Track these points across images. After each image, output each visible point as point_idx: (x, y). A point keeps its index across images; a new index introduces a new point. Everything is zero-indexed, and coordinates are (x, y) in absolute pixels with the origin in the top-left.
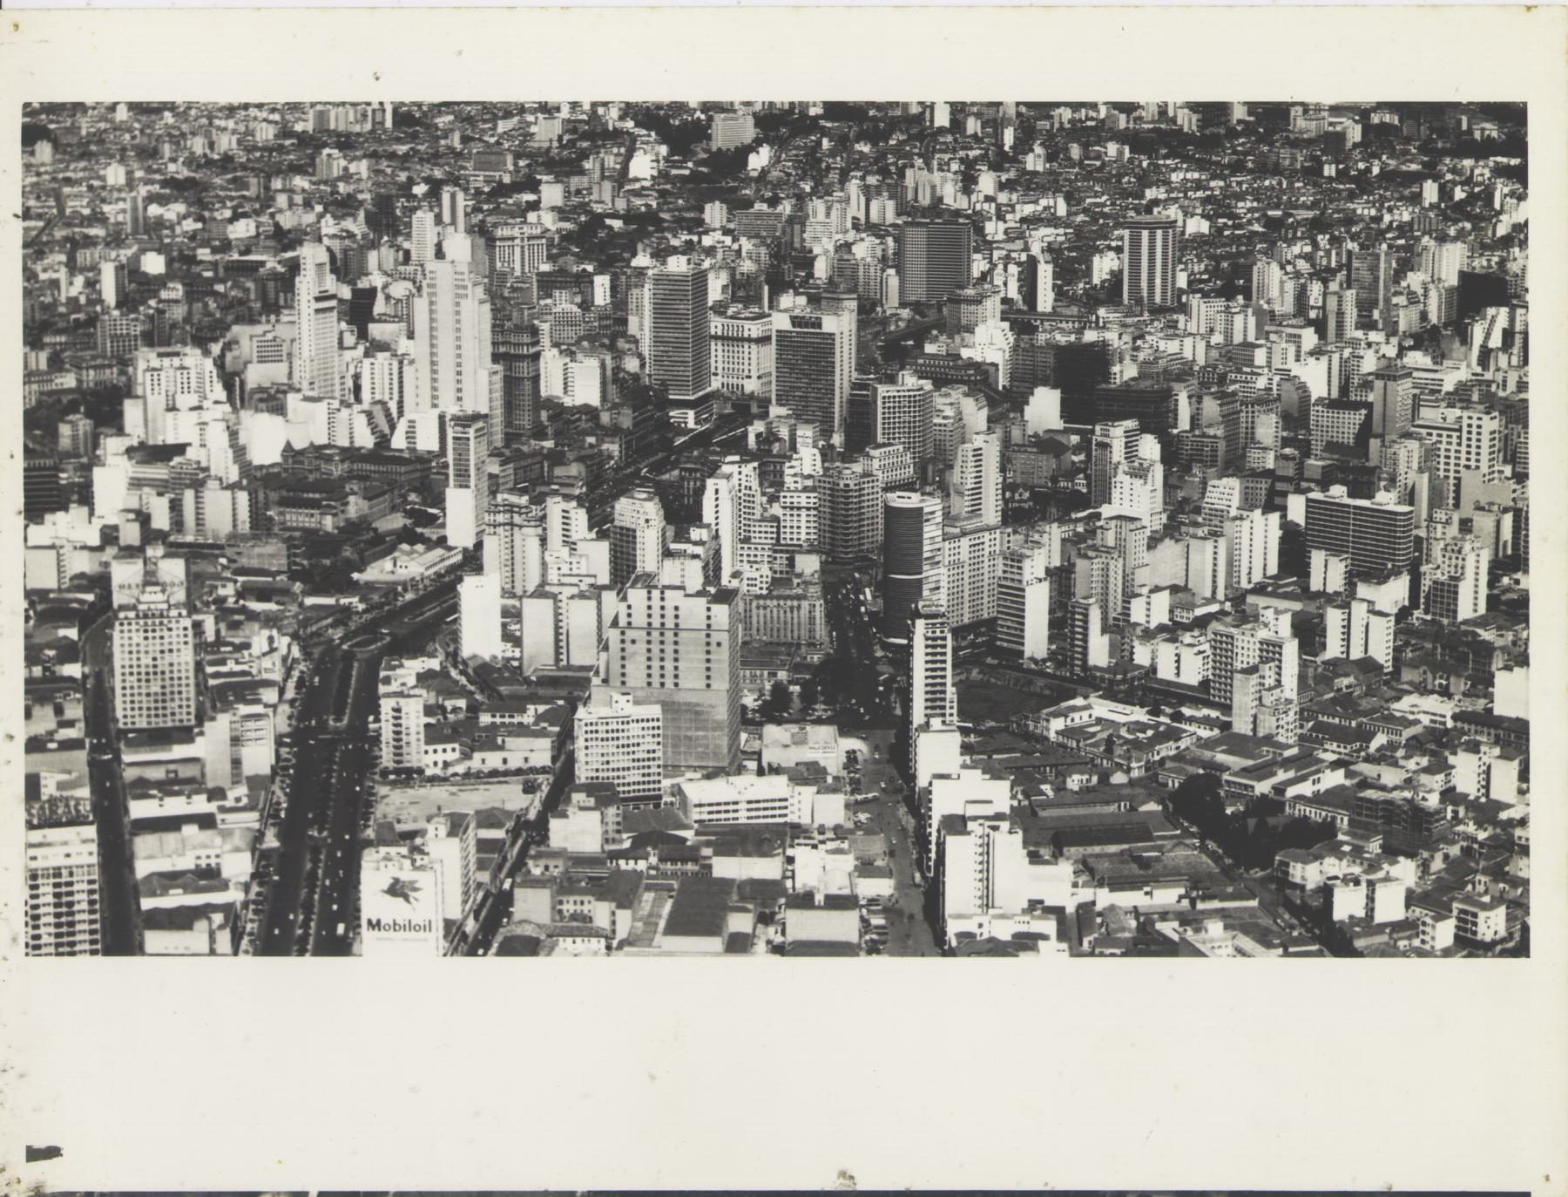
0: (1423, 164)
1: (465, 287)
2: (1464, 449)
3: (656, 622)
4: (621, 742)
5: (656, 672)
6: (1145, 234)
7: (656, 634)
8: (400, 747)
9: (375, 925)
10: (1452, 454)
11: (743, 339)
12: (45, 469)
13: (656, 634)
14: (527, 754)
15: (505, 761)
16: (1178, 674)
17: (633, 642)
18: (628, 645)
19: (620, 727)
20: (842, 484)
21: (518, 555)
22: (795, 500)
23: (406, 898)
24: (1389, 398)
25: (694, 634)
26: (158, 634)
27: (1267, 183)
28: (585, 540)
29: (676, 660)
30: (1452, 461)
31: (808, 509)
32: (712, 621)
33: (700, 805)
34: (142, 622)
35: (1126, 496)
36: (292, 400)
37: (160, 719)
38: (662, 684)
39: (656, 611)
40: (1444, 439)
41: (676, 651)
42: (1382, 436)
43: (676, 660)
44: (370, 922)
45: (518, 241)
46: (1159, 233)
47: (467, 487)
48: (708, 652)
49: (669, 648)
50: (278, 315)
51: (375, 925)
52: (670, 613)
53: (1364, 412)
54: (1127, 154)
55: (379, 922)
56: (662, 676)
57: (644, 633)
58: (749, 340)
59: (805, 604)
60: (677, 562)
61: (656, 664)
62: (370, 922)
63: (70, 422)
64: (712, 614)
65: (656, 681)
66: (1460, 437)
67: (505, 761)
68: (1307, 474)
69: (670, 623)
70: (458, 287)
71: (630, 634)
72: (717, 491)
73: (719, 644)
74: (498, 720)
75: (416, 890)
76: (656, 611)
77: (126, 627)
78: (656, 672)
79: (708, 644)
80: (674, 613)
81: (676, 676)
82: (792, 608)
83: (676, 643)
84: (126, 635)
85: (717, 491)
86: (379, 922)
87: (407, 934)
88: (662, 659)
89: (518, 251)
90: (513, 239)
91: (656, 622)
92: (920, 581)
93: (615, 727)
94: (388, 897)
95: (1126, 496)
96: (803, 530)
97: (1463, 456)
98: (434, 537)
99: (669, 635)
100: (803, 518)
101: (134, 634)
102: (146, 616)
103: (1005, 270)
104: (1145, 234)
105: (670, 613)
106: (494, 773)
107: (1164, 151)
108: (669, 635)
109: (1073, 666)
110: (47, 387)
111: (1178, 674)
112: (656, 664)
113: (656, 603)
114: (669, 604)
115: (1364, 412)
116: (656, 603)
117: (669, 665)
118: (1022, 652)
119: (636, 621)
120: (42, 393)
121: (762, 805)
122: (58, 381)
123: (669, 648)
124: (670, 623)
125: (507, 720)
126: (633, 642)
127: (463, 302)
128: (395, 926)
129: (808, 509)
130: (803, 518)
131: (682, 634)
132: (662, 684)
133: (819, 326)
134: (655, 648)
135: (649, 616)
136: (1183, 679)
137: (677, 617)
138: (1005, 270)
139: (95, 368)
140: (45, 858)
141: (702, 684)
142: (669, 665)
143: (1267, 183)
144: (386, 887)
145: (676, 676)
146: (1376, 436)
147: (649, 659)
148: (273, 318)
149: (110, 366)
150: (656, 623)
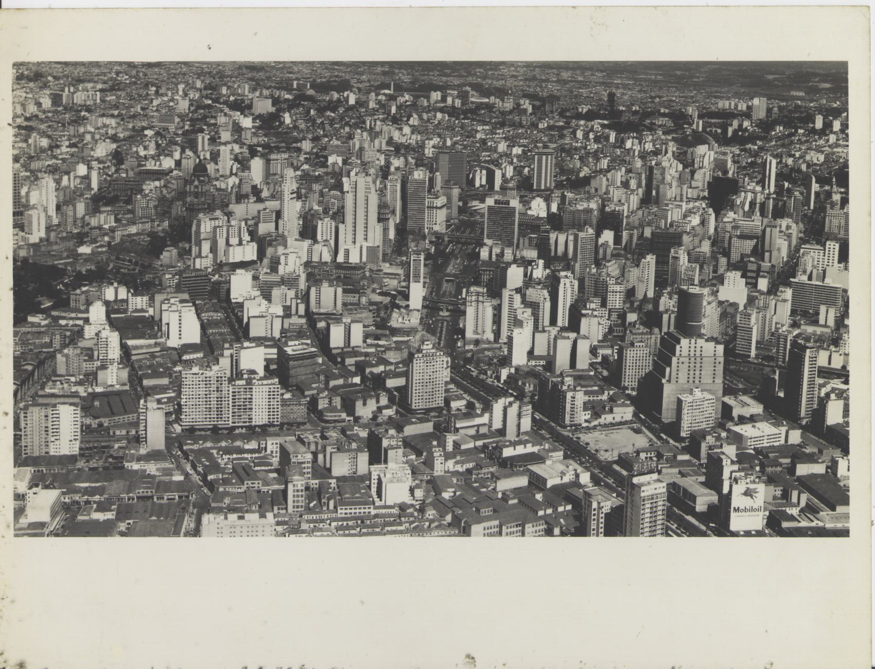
0: (565, 122)
1: (370, 189)
2: (826, 258)
3: (692, 354)
4: (701, 410)
5: (691, 376)
6: (544, 157)
7: (693, 359)
8: (574, 414)
9: (737, 510)
10: (821, 260)
11: (433, 207)
12: (202, 276)
13: (693, 359)
14: (623, 415)
15: (614, 418)
16: (830, 363)
17: (683, 363)
18: (680, 365)
19: (701, 403)
20: (601, 278)
21: (480, 316)
22: (615, 289)
23: (752, 497)
24: (773, 236)
25: (708, 359)
26: (432, 364)
27: (520, 131)
28: (520, 308)
29: (701, 370)
30: (821, 263)
31: (620, 292)
32: (716, 353)
33: (751, 438)
34: (425, 359)
35: (732, 282)
36: (307, 243)
37: (431, 403)
38: (694, 382)
39: (692, 349)
40: (817, 254)
41: (701, 367)
42: (770, 252)
43: (701, 370)
44: (734, 508)
45: (279, 161)
46: (550, 156)
47: (419, 282)
48: (715, 367)
49: (698, 365)
50: (248, 199)
51: (737, 510)
52: (698, 349)
53: (755, 240)
54: (447, 118)
55: (738, 508)
56: (694, 378)
57: (688, 359)
58: (437, 208)
59: (653, 337)
60: (588, 319)
61: (692, 373)
62: (734, 508)
63: (168, 251)
64: (716, 349)
65: (691, 380)
66: (824, 253)
67: (614, 418)
68: (762, 269)
69: (698, 354)
70: (366, 188)
71: (681, 360)
72: (565, 284)
73: (720, 363)
74: (591, 398)
75: (757, 492)
76: (692, 349)
77: (418, 361)
78: (691, 376)
79: (715, 363)
80: (700, 349)
81: (700, 378)
82: (648, 338)
83: (701, 363)
84: (418, 365)
85: (565, 284)
86: (738, 508)
87: (751, 513)
88: (695, 370)
89: (279, 165)
90: (277, 160)
91: (692, 354)
92: (700, 325)
93: (698, 403)
94: (744, 496)
95: (732, 282)
96: (618, 302)
97: (826, 261)
98: (404, 305)
99: (698, 359)
100: (618, 296)
101: (422, 364)
102: (426, 356)
103: (481, 172)
104: (544, 157)
105: (698, 349)
106: (612, 424)
107: (462, 116)
108: (698, 359)
109: (778, 361)
110: (126, 233)
111: (830, 363)
112: (692, 373)
113: (693, 345)
114: (698, 346)
115: (755, 240)
116: (693, 345)
117: (697, 373)
118: (750, 356)
119: (683, 354)
120: (123, 236)
121: (772, 437)
122: (129, 230)
123: (698, 365)
124: (698, 354)
125: (595, 398)
126: (683, 363)
127: (369, 195)
128: (745, 510)
129: (620, 292)
130: (618, 296)
131: (704, 359)
132: (694, 382)
133: (508, 204)
134: (692, 365)
135: (689, 351)
136: (833, 366)
137: (701, 351)
138: (481, 172)
139: (142, 223)
140: (647, 491)
141: (710, 381)
142: (697, 373)
143: (520, 131)
144: (743, 492)
145: (700, 378)
146: (767, 251)
147: (689, 370)
148: (246, 201)
149: (148, 222)
150: (692, 355)
